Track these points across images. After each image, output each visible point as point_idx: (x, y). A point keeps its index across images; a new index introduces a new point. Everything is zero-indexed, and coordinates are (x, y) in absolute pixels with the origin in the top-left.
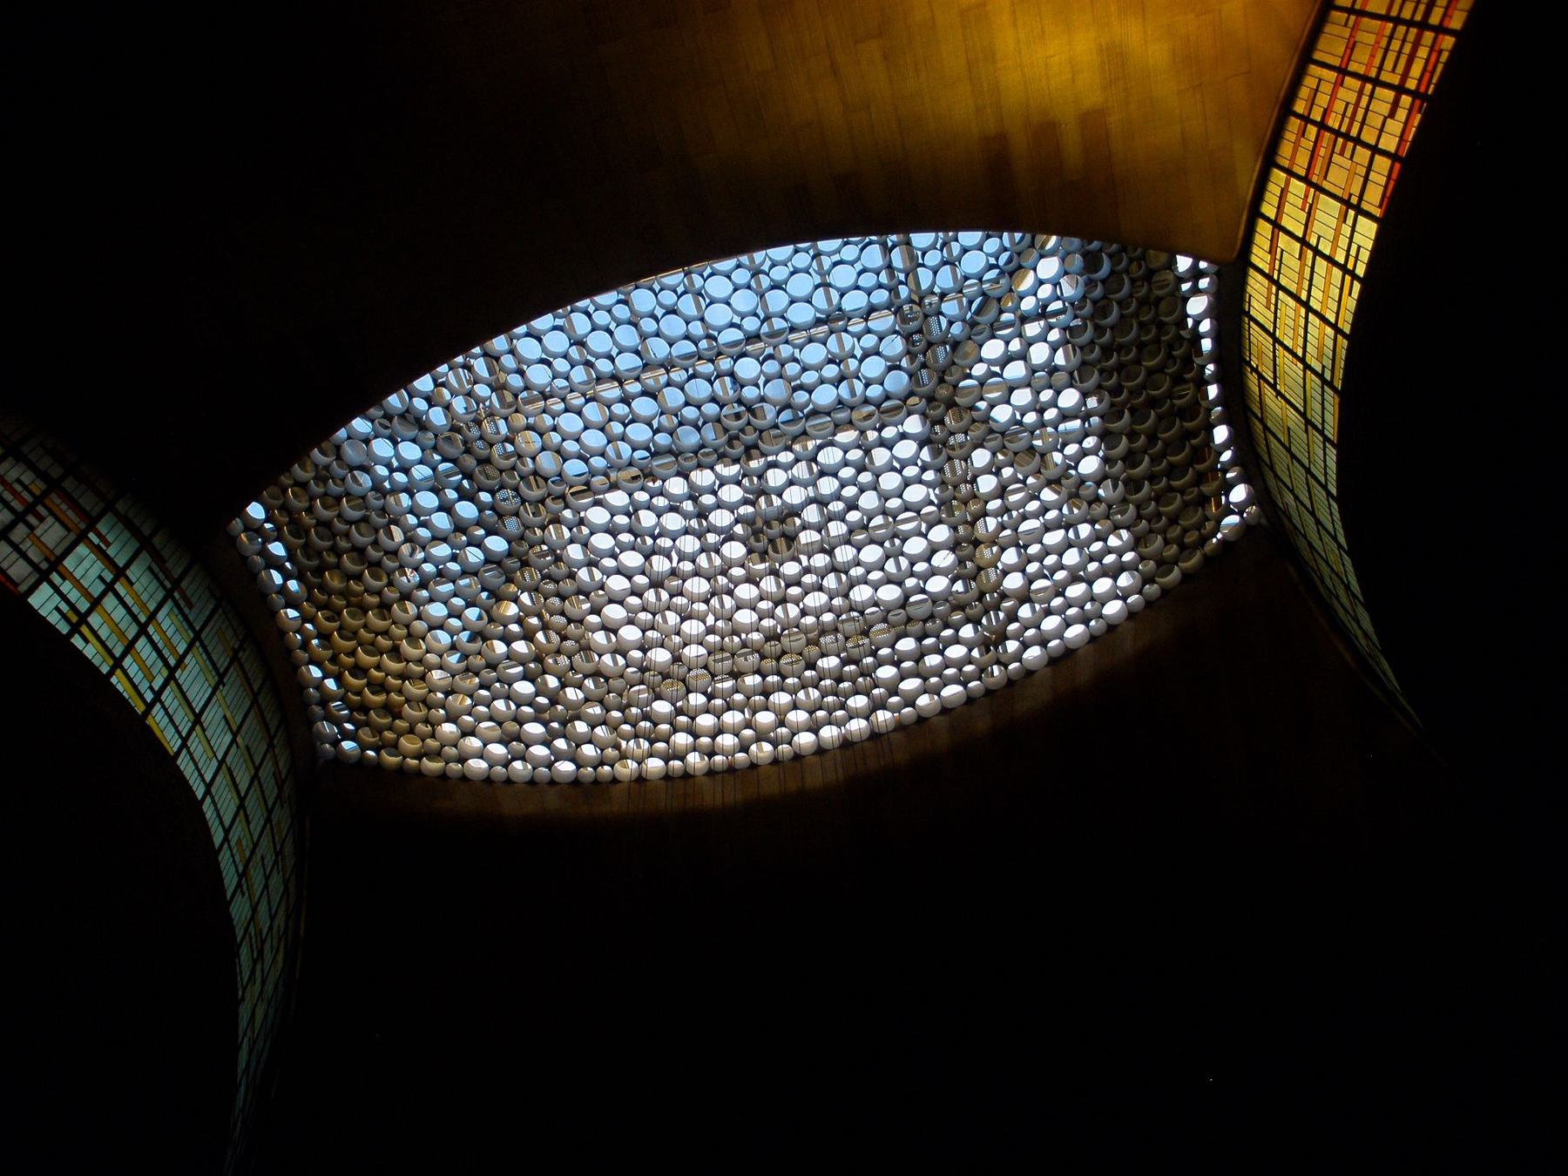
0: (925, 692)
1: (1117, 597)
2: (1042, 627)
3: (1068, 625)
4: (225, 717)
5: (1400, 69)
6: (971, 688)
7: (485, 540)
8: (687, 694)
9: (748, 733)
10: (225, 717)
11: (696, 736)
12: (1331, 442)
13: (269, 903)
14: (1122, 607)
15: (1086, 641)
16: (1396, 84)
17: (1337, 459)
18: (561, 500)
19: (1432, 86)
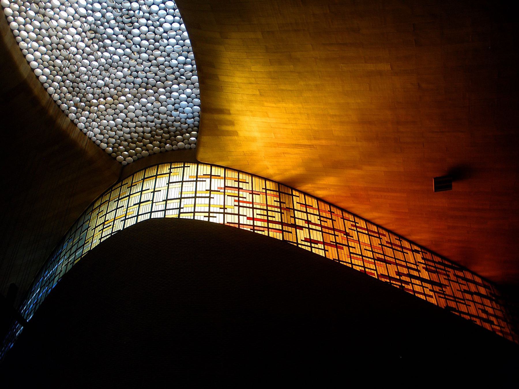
0: (81, 55)
1: (75, 10)
2: (61, 12)
3: (111, 46)
4: (352, 237)
5: (259, 217)
6: (21, 27)
7: (21, 42)
8: (113, 110)
9: (22, 26)
10: (352, 237)
11: (76, 12)
12: (112, 190)
13: (59, 276)
14: (184, 60)
15: (6, 15)
16: (267, 223)
17: (106, 239)
18: (210, 166)
19: (292, 244)
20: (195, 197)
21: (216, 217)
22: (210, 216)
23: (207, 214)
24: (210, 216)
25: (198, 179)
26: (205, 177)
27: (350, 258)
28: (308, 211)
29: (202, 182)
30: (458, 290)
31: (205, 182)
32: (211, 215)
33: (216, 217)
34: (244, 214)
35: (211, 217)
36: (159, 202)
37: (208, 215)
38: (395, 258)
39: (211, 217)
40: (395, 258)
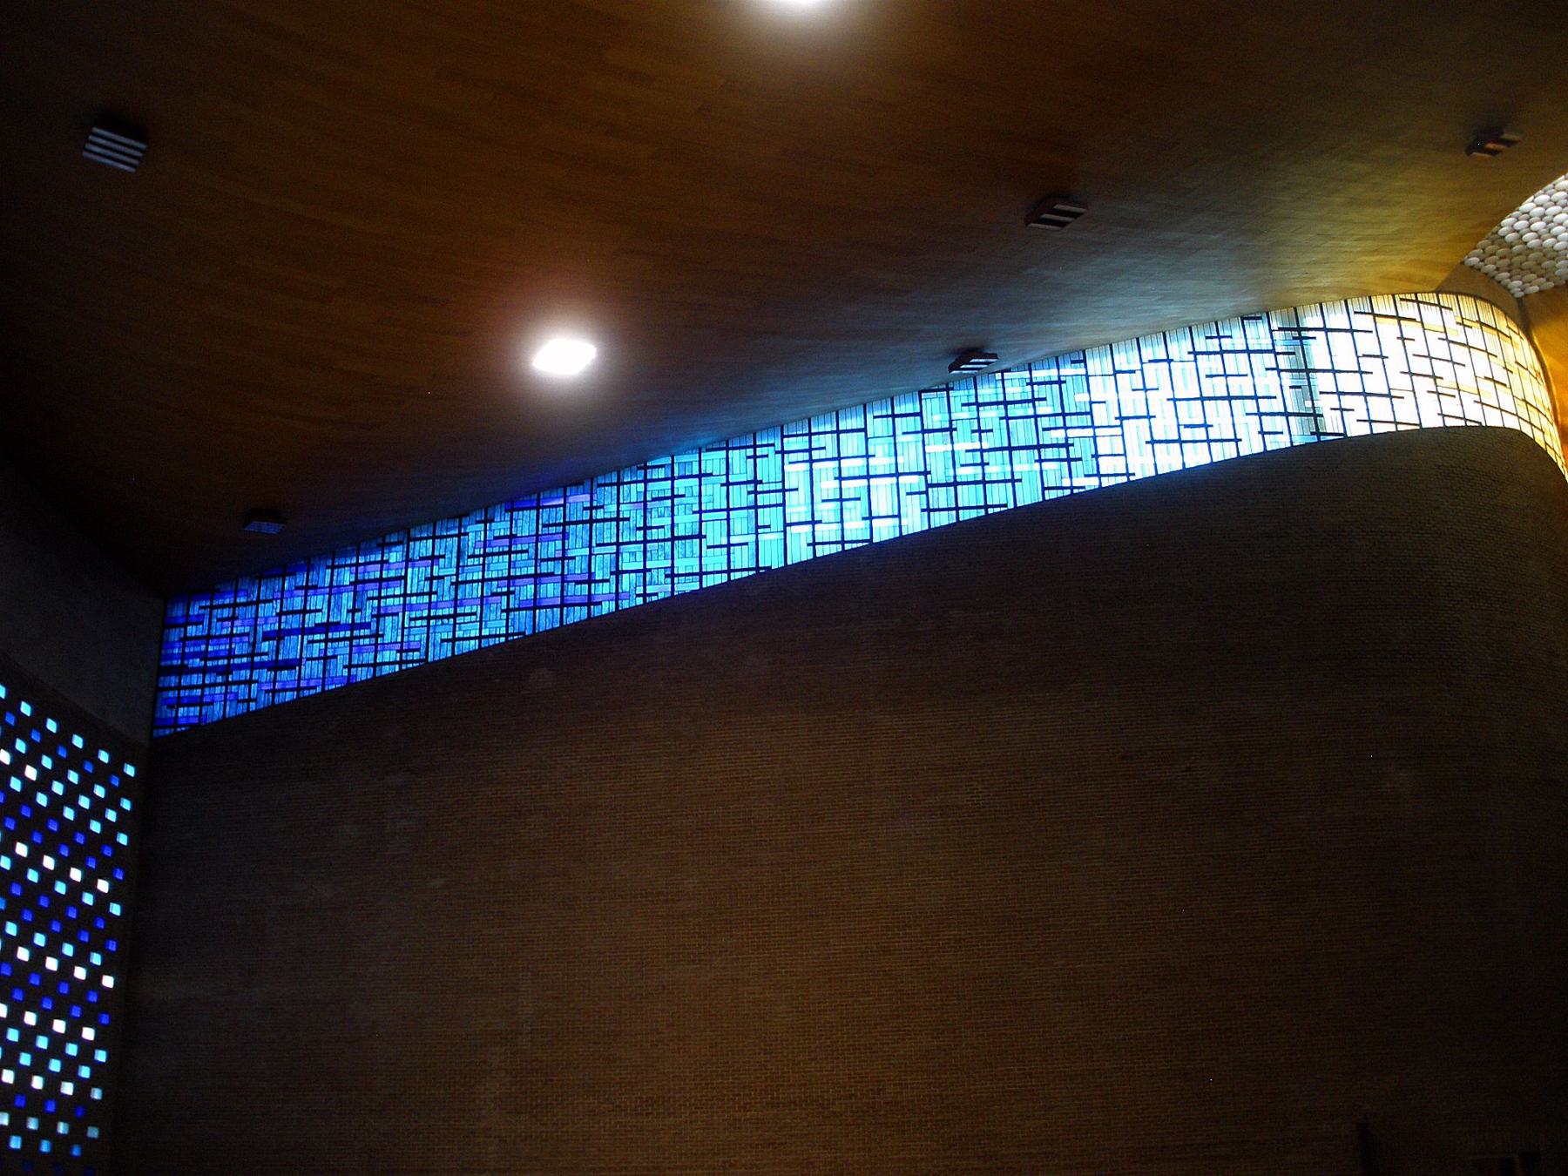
20: (728, 510)
21: (767, 456)
22: (1013, 452)
23: (816, 454)
24: (1013, 452)
25: (724, 516)
26: (605, 550)
27: (367, 585)
28: (1420, 299)
29: (772, 503)
30: (1512, 372)
31: (991, 433)
32: (806, 456)
33: (767, 456)
34: (1405, 302)
35: (816, 434)
36: (1445, 332)
37: (846, 545)
38: (1418, 302)
39: (816, 434)
40: (1418, 302)
